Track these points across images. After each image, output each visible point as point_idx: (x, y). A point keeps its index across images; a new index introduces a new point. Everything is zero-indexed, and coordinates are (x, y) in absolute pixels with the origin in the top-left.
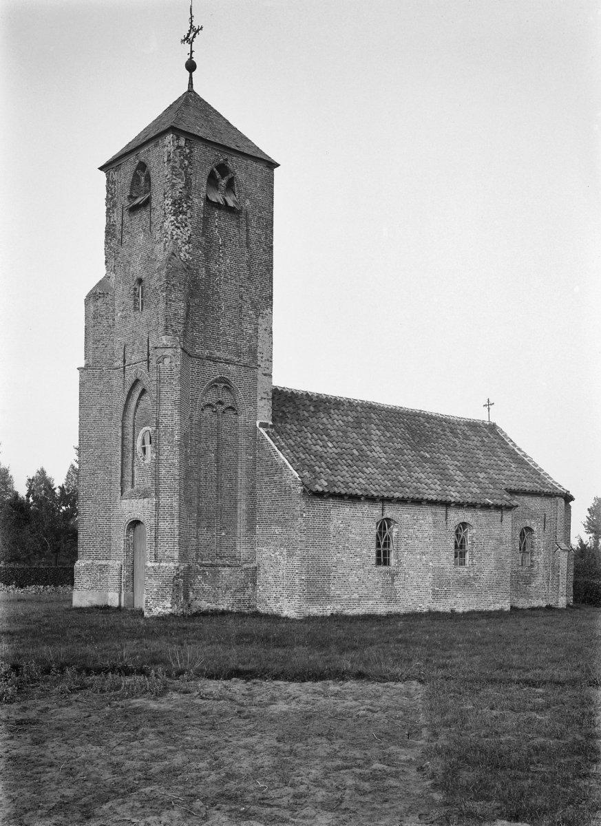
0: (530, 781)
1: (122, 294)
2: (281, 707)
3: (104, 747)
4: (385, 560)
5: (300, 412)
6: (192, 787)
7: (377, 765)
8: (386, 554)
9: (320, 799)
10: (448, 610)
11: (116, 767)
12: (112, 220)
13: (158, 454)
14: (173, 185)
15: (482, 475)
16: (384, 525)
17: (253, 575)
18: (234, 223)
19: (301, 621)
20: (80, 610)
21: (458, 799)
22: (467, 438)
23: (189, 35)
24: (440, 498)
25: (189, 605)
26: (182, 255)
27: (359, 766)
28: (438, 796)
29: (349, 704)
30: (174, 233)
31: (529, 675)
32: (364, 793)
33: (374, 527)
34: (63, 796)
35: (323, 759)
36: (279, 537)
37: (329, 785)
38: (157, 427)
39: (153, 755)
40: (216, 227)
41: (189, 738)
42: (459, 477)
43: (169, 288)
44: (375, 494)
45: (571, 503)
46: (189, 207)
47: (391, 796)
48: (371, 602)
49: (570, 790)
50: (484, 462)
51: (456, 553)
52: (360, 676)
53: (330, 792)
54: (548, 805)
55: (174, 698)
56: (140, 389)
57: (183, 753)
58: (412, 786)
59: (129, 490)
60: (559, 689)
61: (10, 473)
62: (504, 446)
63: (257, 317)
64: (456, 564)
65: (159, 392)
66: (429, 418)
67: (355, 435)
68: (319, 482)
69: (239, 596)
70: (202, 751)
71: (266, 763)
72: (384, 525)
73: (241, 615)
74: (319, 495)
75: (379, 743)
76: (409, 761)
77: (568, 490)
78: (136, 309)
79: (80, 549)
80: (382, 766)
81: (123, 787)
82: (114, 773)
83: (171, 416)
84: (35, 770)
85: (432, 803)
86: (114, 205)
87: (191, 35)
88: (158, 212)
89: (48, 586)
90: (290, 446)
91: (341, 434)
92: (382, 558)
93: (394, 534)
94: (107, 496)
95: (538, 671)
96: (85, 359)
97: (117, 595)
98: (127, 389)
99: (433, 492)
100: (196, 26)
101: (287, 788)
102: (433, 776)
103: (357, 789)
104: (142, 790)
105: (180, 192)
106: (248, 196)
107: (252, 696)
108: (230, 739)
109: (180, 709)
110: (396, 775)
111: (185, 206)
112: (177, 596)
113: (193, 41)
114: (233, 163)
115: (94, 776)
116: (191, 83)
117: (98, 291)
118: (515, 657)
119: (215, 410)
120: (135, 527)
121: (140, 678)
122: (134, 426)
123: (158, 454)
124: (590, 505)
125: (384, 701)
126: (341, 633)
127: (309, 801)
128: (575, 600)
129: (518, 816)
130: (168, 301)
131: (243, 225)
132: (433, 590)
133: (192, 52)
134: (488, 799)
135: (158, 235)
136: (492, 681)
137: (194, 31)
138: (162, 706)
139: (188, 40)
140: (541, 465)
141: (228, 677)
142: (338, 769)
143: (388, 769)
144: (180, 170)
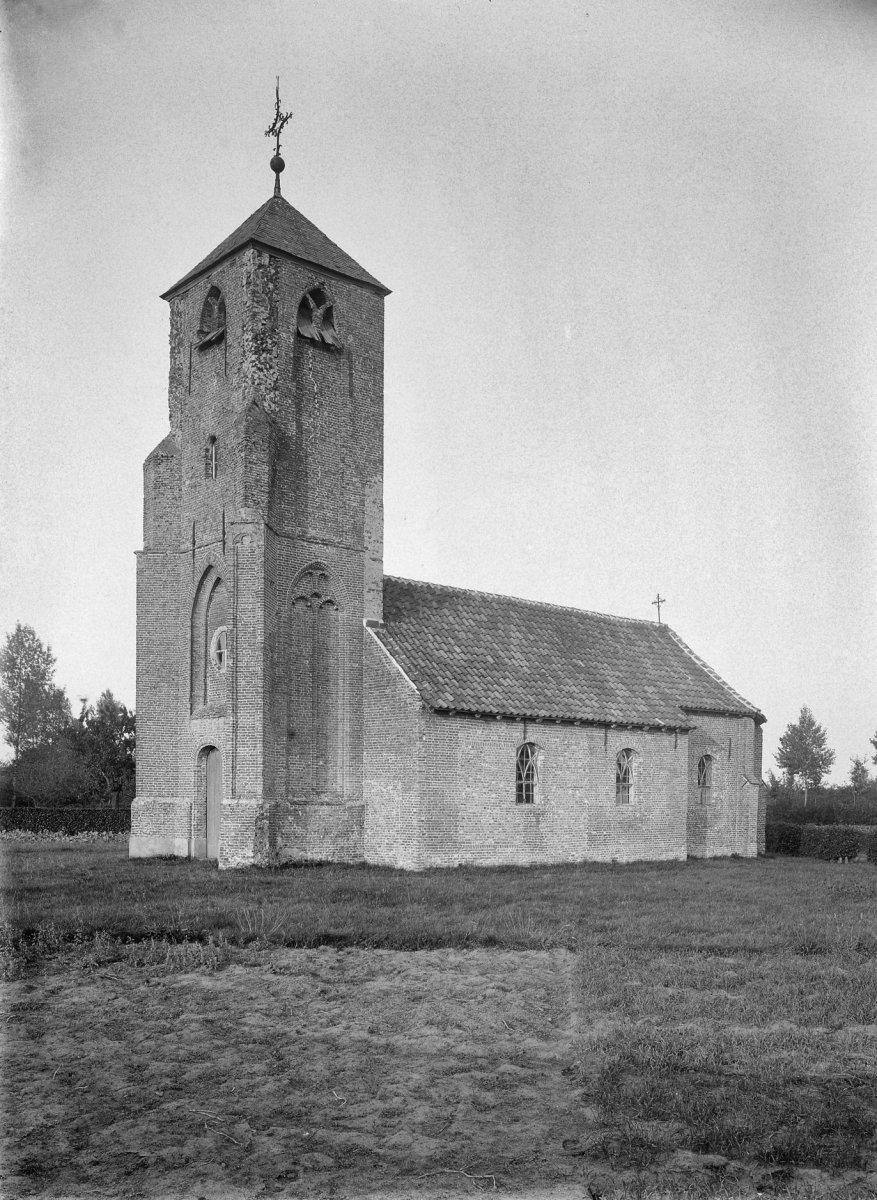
0: (723, 1089)
1: (191, 458)
2: (381, 983)
3: (124, 1043)
4: (528, 797)
5: (420, 608)
6: (238, 1102)
7: (506, 1067)
8: (529, 788)
9: (420, 1118)
10: (608, 859)
11: (136, 1073)
12: (178, 363)
13: (236, 660)
14: (255, 315)
15: (650, 689)
16: (525, 752)
17: (359, 815)
18: (334, 365)
19: (420, 874)
20: (138, 861)
21: (619, 1117)
22: (631, 643)
23: (274, 125)
24: (597, 718)
25: (277, 854)
26: (266, 404)
27: (481, 1068)
28: (591, 1113)
29: (472, 979)
30: (256, 376)
31: (715, 941)
32: (487, 1108)
33: (514, 754)
34: (48, 1116)
35: (431, 1057)
36: (392, 766)
37: (435, 1096)
38: (235, 626)
39: (191, 1053)
40: (310, 369)
41: (246, 1029)
42: (621, 691)
43: (249, 447)
44: (515, 712)
45: (762, 726)
46: (275, 343)
47: (524, 1113)
48: (510, 849)
49: (780, 1103)
50: (653, 673)
51: (618, 788)
52: (490, 942)
53: (436, 1107)
54: (751, 1127)
55: (237, 972)
56: (212, 578)
57: (234, 1050)
58: (556, 1097)
59: (200, 707)
60: (755, 959)
61: (66, 696)
62: (678, 653)
63: (364, 485)
64: (618, 801)
65: (236, 580)
66: (583, 617)
67: (490, 639)
68: (443, 697)
69: (341, 842)
70: (263, 1047)
71: (349, 1065)
72: (525, 752)
73: (345, 867)
74: (443, 712)
75: (510, 1035)
76: (553, 1061)
77: (759, 708)
78: (208, 476)
79: (138, 783)
80: (513, 1067)
81: (139, 1102)
82: (130, 1080)
83: (253, 613)
84: (18, 1076)
85: (582, 1124)
86: (180, 343)
87: (278, 125)
88: (236, 350)
89: (104, 833)
90: (405, 651)
91: (471, 636)
92: (524, 794)
93: (539, 763)
94: (172, 715)
95: (725, 935)
96: (144, 540)
97: (186, 841)
98: (198, 578)
99: (588, 710)
100: (284, 111)
101: (374, 1101)
102: (585, 1080)
103: (476, 1103)
104: (165, 1106)
105: (263, 324)
106: (350, 330)
107: (343, 970)
108: (304, 1030)
109: (242, 988)
110: (530, 1081)
111: (270, 341)
112: (261, 843)
113: (280, 132)
114: (334, 290)
115: (101, 1084)
116: (278, 187)
117: (161, 453)
118: (696, 917)
120: (208, 754)
121: (196, 946)
122: (206, 625)
123: (236, 660)
124: (782, 734)
125: (520, 976)
126: (470, 888)
127: (405, 1120)
128: (767, 848)
129: (708, 1145)
130: (248, 463)
131: (345, 368)
132: (590, 834)
133: (279, 146)
134: (663, 1117)
135: (235, 380)
136: (666, 948)
137: (282, 119)
138: (219, 983)
139: (274, 131)
140: (725, 678)
141: (316, 944)
142: (451, 1072)
143: (522, 1072)
144: (263, 295)
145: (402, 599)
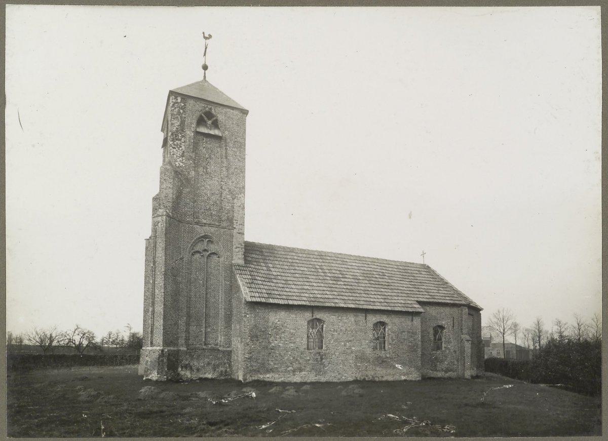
18: (217, 145)
63: (233, 199)
119: (202, 255)
145: (250, 249)
